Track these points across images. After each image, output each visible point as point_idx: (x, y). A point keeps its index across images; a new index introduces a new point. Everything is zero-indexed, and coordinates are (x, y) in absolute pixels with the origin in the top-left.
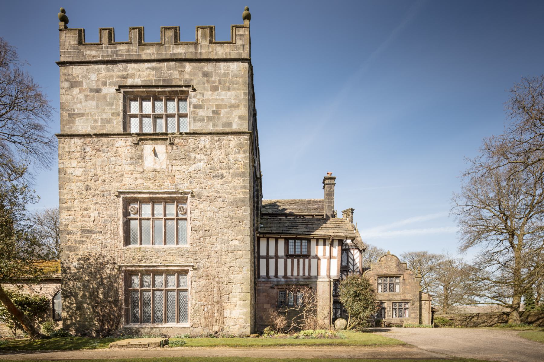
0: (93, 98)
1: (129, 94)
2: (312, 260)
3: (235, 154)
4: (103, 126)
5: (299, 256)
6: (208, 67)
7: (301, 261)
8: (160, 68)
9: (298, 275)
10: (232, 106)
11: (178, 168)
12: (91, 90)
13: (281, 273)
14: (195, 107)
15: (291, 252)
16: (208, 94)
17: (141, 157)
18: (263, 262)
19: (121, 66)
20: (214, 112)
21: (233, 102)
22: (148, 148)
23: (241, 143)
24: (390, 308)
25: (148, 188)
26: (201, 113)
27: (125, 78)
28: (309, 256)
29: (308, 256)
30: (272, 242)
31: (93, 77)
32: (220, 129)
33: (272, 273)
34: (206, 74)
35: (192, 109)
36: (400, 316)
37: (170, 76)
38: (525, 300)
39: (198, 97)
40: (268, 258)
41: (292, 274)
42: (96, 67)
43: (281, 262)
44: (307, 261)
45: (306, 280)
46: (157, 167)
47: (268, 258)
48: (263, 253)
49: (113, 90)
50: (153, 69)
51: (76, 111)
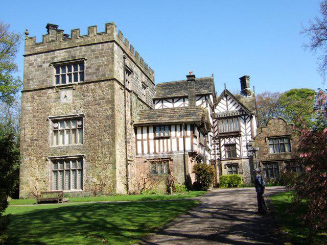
2: (172, 140)
6: (93, 47)
12: (38, 66)
13: (152, 151)
16: (94, 61)
19: (52, 53)
31: (39, 60)
32: (100, 78)
33: (146, 151)
34: (93, 51)
38: (5, 239)
41: (159, 151)
43: (152, 142)
44: (169, 140)
51: (31, 78)
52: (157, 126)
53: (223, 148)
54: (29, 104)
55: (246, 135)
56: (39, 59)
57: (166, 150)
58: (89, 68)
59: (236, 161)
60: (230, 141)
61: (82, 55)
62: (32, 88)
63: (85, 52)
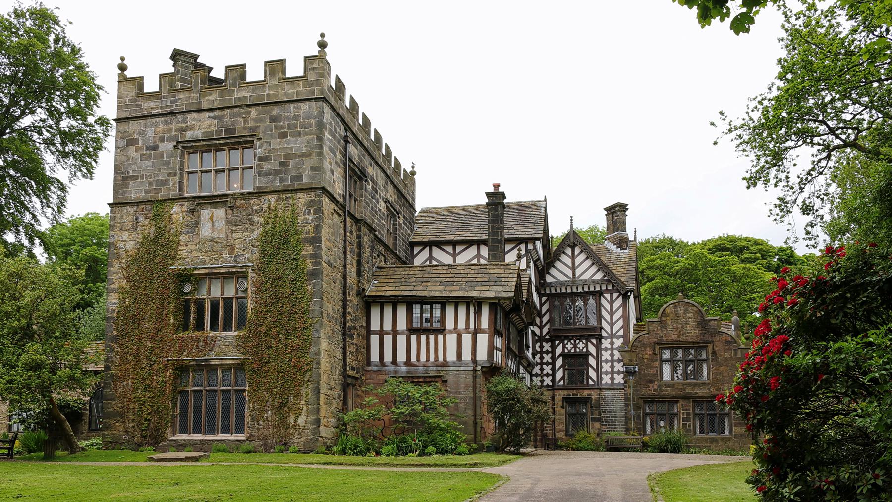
0: (149, 157)
1: (189, 147)
2: (448, 335)
3: (304, 214)
4: (158, 190)
5: (428, 331)
6: (275, 111)
7: (432, 337)
8: (223, 116)
9: (428, 359)
10: (303, 155)
11: (239, 235)
12: (148, 148)
13: (402, 357)
14: (261, 159)
15: (416, 325)
16: (276, 143)
17: (197, 224)
18: (374, 340)
19: (180, 117)
20: (282, 164)
21: (304, 150)
22: (205, 213)
23: (312, 201)
24: (688, 414)
25: (204, 262)
26: (267, 166)
27: (184, 131)
28: (444, 329)
29: (442, 330)
30: (388, 311)
31: (150, 132)
33: (388, 358)
34: (273, 119)
35: (257, 162)
36: (712, 430)
37: (233, 125)
39: (264, 147)
40: (381, 333)
41: (418, 360)
42: (154, 120)
43: (402, 340)
44: (440, 337)
45: (439, 368)
46: (215, 235)
47: (381, 333)
48: (375, 325)
49: (170, 146)
50: (215, 118)
51: (131, 174)
53: (559, 362)
55: (612, 336)
56: (151, 131)
57: (432, 358)
59: (586, 393)
60: (575, 346)
61: (250, 128)
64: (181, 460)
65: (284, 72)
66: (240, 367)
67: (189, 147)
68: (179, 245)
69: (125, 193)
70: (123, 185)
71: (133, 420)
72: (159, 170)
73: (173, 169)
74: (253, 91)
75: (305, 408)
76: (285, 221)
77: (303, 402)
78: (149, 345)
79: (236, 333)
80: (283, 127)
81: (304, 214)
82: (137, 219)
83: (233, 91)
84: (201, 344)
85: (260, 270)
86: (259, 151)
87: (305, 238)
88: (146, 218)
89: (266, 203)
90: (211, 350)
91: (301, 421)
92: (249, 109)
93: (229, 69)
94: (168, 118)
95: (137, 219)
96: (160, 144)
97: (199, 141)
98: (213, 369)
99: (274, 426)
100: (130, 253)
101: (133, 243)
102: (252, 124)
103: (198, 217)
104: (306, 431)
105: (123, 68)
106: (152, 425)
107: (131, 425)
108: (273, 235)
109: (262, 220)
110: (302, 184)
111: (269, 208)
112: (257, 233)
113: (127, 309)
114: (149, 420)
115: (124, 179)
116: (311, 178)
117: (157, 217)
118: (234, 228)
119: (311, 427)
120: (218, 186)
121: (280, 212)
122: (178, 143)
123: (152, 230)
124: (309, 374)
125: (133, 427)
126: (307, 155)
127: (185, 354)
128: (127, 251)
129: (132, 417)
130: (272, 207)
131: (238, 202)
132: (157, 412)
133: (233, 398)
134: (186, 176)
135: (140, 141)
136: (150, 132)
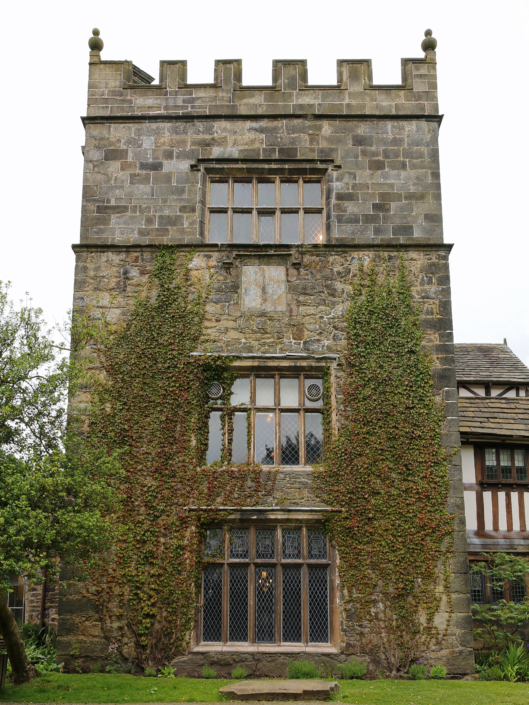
0: (146, 180)
4: (163, 231)
6: (363, 129)
7: (502, 495)
8: (275, 129)
10: (410, 196)
11: (311, 310)
12: (143, 166)
16: (364, 176)
17: (235, 288)
19: (200, 125)
22: (251, 273)
23: (433, 264)
25: (250, 349)
26: (351, 208)
27: (208, 145)
31: (148, 143)
34: (359, 141)
41: (496, 527)
42: (154, 126)
46: (269, 308)
49: (185, 165)
50: (261, 130)
51: (113, 203)
52: (491, 445)
54: (105, 299)
56: (150, 141)
57: (516, 527)
58: (350, 197)
61: (322, 151)
62: (118, 238)
63: (329, 140)
64: (295, 697)
65: (370, 78)
66: (320, 526)
67: (220, 171)
68: (203, 318)
69: (101, 231)
70: (98, 219)
71: (120, 617)
72: (165, 201)
73: (189, 201)
74: (324, 98)
75: (444, 598)
76: (390, 292)
77: (440, 588)
78: (149, 482)
79: (309, 468)
80: (377, 154)
81: (422, 284)
82: (126, 273)
83: (291, 95)
84: (249, 483)
85: (351, 365)
86: (337, 186)
87: (426, 321)
88: (142, 273)
89: (356, 262)
90: (269, 493)
91: (440, 620)
92: (318, 123)
93: (280, 66)
94: (181, 125)
95: (126, 273)
96: (165, 162)
97: (236, 161)
98: (266, 526)
99: (389, 629)
100: (113, 328)
101: (118, 311)
102: (323, 144)
103: (238, 276)
104: (452, 639)
105: (96, 45)
106: (157, 626)
107: (116, 625)
108: (371, 313)
109: (349, 288)
110: (413, 239)
111: (361, 270)
112: (341, 309)
113: (110, 418)
114: (153, 616)
115: (99, 209)
116: (425, 230)
117: (162, 273)
118: (301, 298)
119: (458, 631)
120: (268, 232)
121: (381, 279)
122: (200, 161)
123: (154, 293)
124: (447, 540)
125: (121, 628)
126: (421, 197)
127: (219, 500)
128: (107, 324)
129: (117, 611)
130: (365, 269)
131: (307, 259)
132: (167, 602)
133: (304, 575)
134: (207, 213)
135: (130, 155)
136: (148, 143)
